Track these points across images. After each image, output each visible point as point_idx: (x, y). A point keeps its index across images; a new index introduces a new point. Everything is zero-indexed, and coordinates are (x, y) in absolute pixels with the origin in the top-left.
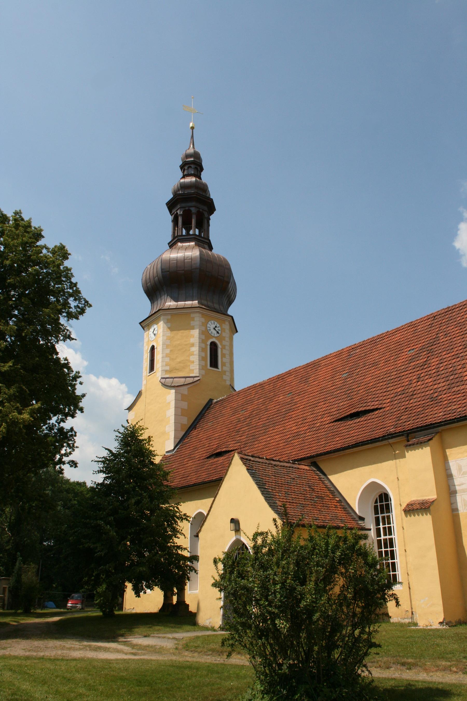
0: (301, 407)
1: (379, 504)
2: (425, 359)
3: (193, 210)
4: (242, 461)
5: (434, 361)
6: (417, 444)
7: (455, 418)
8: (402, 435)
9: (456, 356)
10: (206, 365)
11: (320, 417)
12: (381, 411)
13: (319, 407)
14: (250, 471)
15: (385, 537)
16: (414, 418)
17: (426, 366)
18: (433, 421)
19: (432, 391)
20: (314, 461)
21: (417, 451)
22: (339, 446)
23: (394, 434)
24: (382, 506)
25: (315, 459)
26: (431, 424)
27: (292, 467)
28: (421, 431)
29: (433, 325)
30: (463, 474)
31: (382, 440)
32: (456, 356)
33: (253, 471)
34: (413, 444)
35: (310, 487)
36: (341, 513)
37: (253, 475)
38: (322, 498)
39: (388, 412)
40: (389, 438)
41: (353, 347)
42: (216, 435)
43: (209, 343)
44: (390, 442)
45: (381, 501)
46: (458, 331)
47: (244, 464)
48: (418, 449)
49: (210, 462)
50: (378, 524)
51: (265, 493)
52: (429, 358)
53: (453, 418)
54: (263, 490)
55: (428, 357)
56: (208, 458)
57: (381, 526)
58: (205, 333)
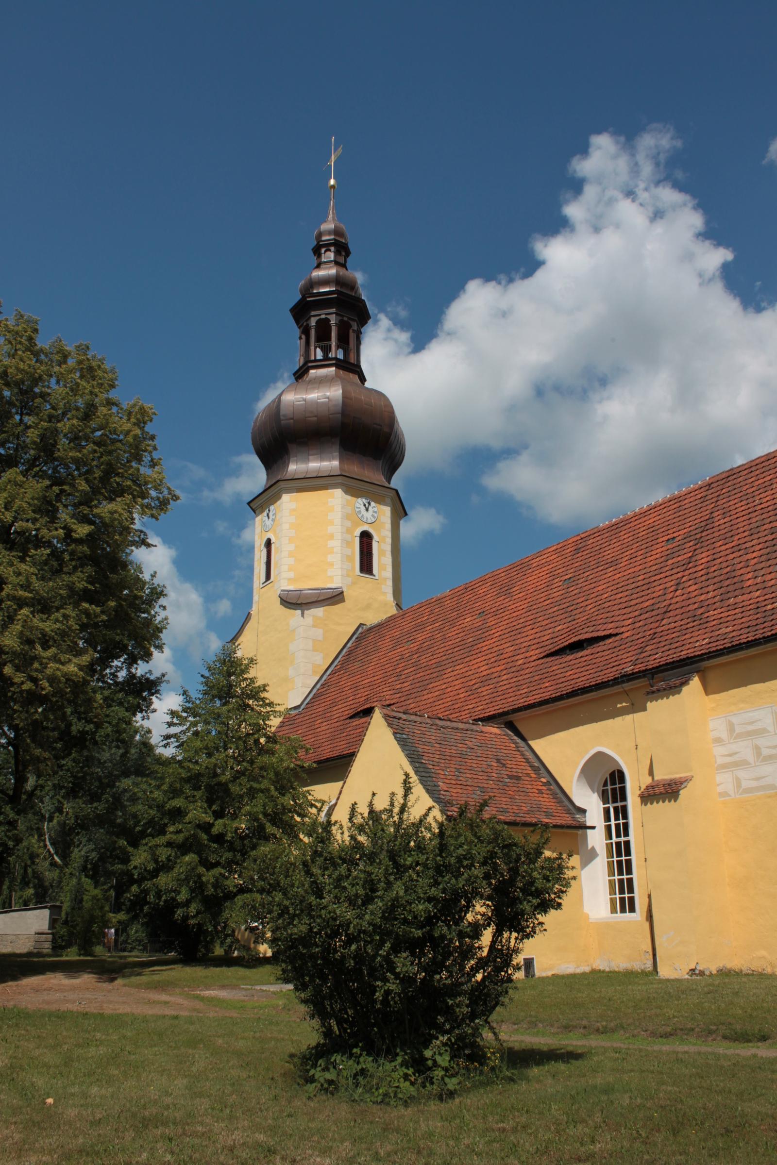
0: (496, 635)
1: (609, 787)
2: (690, 554)
3: (333, 320)
4: (386, 720)
5: (703, 557)
6: (665, 689)
7: (725, 648)
8: (644, 676)
9: (737, 548)
10: (353, 568)
11: (524, 650)
12: (618, 638)
13: (524, 635)
14: (398, 736)
15: (619, 840)
16: (664, 649)
17: (691, 565)
18: (691, 653)
19: (696, 606)
20: (507, 720)
21: (660, 701)
22: (546, 696)
23: (630, 675)
24: (614, 791)
25: (511, 717)
26: (688, 658)
27: (472, 730)
28: (672, 669)
29: (707, 498)
30: (735, 738)
31: (612, 686)
32: (737, 548)
33: (404, 736)
34: (658, 690)
35: (498, 761)
36: (546, 801)
37: (403, 743)
38: (518, 778)
39: (627, 640)
40: (623, 682)
41: (582, 536)
42: (366, 681)
43: (358, 533)
44: (626, 689)
45: (613, 783)
46: (743, 508)
47: (390, 725)
48: (662, 699)
49: (354, 724)
50: (607, 818)
51: (422, 770)
52: (697, 552)
53: (722, 647)
54: (417, 765)
55: (695, 550)
56: (351, 718)
57: (613, 823)
58: (352, 517)
